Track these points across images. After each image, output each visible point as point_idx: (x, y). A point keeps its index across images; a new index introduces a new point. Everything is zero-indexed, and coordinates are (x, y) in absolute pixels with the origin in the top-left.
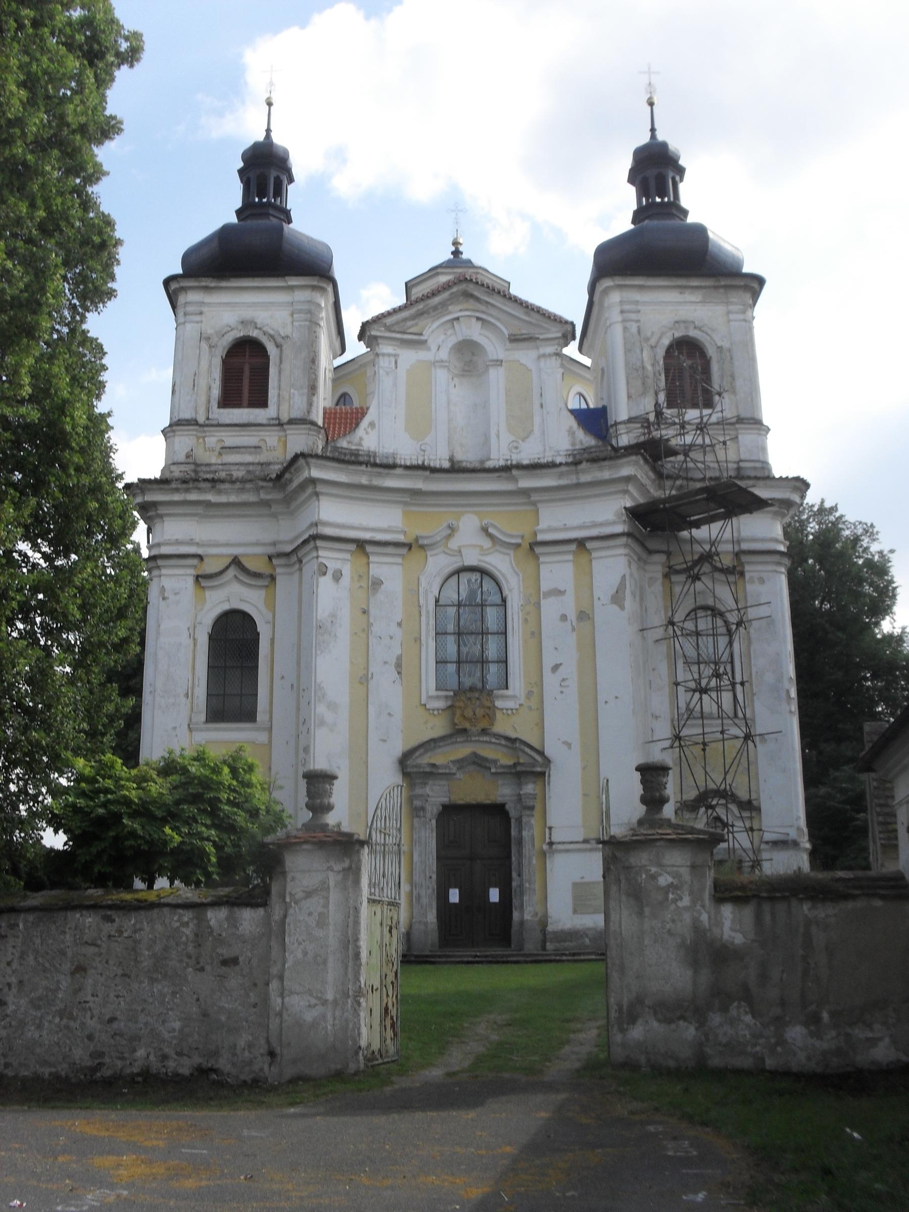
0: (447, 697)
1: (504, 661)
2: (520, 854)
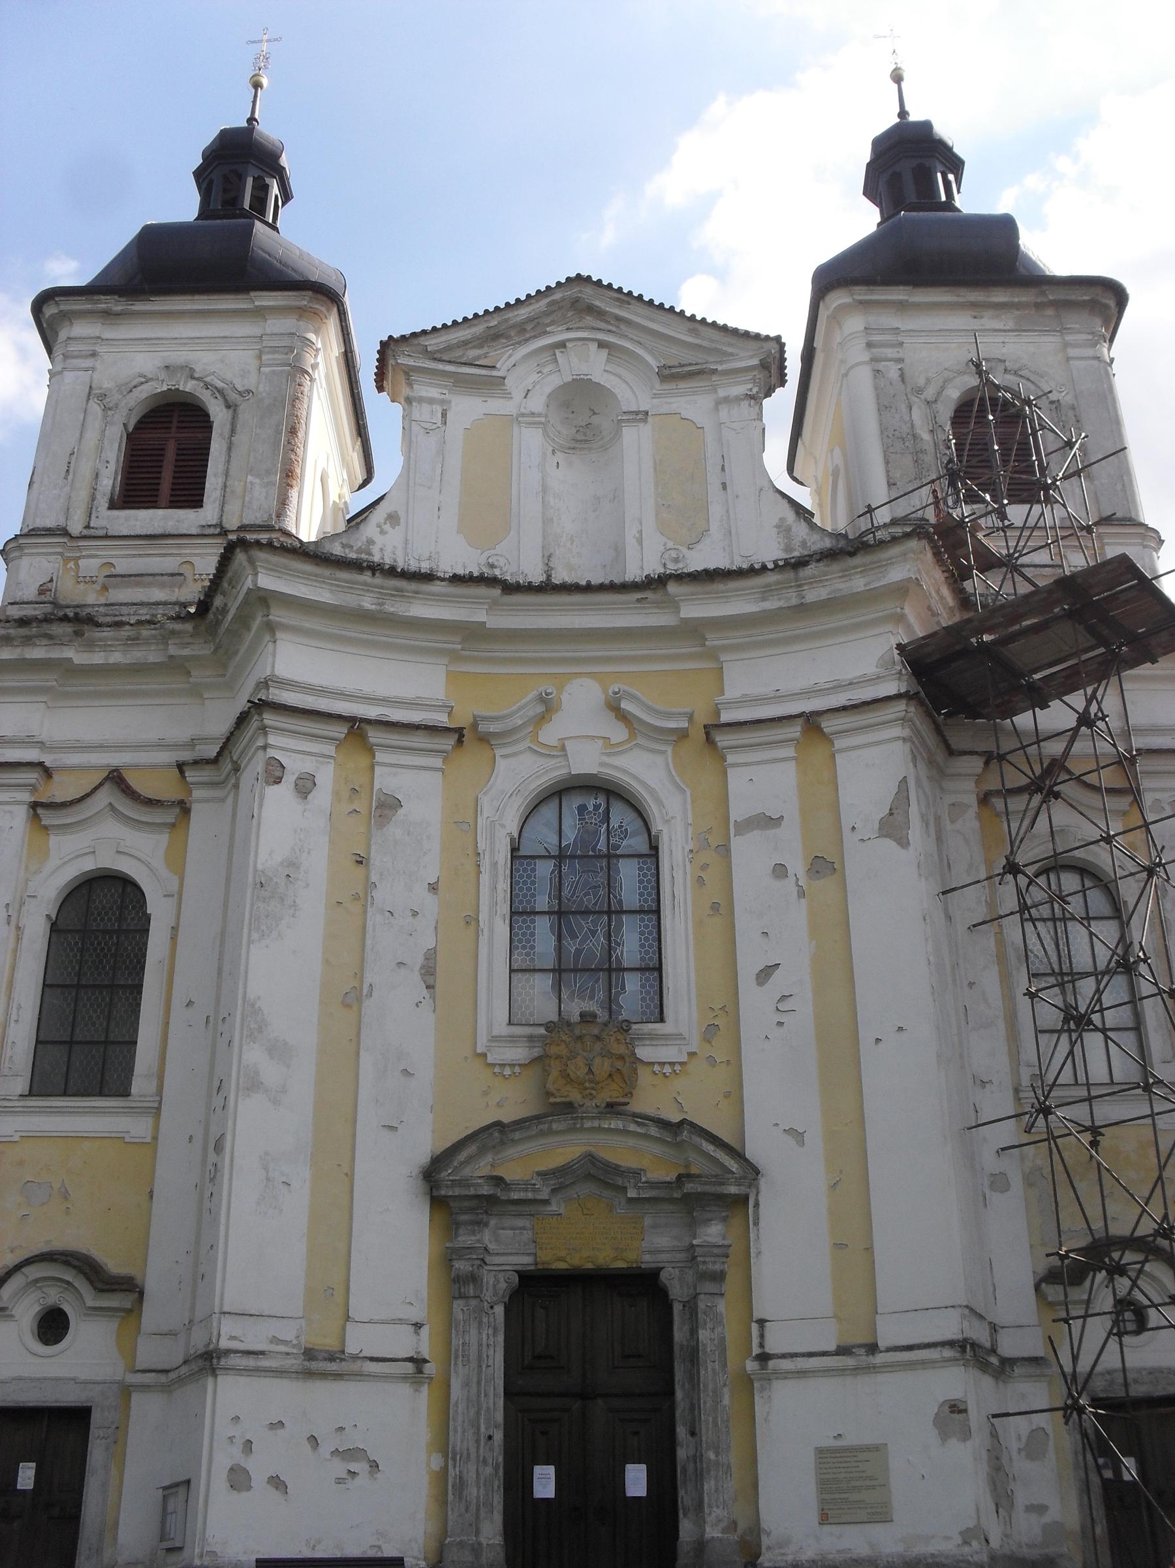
0: (531, 1038)
1: (655, 969)
2: (694, 1381)
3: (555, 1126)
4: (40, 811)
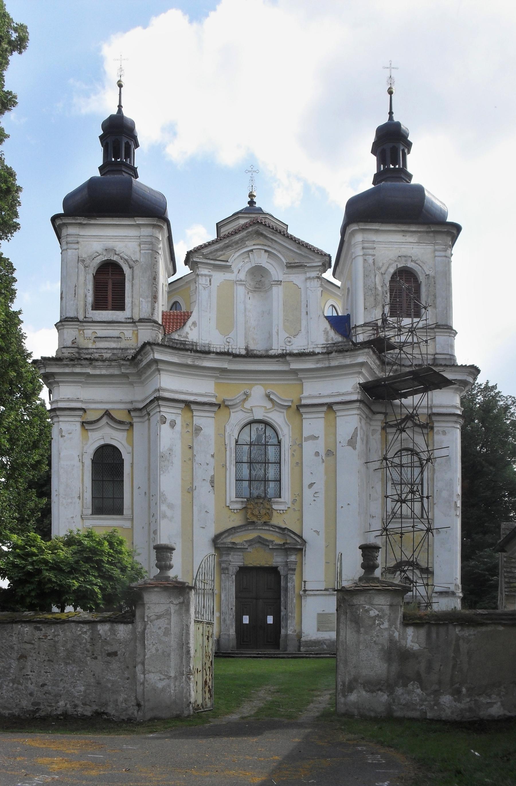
0: (242, 502)
1: (279, 481)
2: (286, 596)
3: (249, 528)
4: (84, 424)
